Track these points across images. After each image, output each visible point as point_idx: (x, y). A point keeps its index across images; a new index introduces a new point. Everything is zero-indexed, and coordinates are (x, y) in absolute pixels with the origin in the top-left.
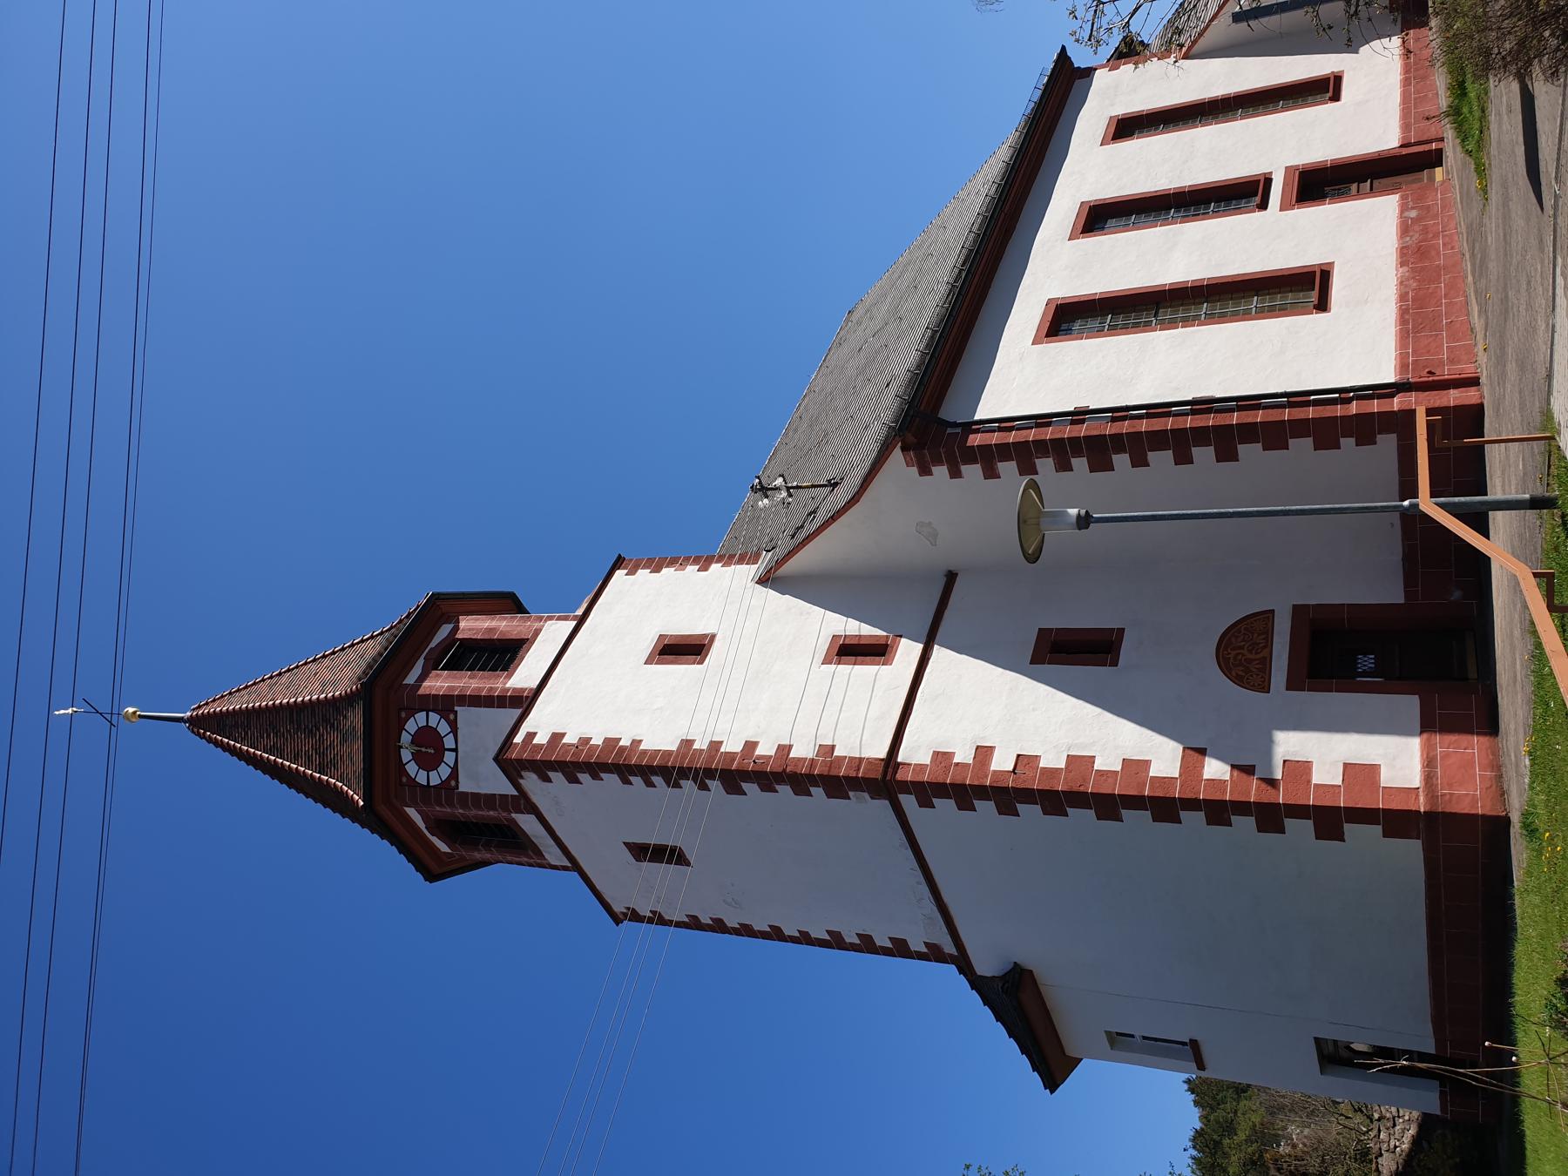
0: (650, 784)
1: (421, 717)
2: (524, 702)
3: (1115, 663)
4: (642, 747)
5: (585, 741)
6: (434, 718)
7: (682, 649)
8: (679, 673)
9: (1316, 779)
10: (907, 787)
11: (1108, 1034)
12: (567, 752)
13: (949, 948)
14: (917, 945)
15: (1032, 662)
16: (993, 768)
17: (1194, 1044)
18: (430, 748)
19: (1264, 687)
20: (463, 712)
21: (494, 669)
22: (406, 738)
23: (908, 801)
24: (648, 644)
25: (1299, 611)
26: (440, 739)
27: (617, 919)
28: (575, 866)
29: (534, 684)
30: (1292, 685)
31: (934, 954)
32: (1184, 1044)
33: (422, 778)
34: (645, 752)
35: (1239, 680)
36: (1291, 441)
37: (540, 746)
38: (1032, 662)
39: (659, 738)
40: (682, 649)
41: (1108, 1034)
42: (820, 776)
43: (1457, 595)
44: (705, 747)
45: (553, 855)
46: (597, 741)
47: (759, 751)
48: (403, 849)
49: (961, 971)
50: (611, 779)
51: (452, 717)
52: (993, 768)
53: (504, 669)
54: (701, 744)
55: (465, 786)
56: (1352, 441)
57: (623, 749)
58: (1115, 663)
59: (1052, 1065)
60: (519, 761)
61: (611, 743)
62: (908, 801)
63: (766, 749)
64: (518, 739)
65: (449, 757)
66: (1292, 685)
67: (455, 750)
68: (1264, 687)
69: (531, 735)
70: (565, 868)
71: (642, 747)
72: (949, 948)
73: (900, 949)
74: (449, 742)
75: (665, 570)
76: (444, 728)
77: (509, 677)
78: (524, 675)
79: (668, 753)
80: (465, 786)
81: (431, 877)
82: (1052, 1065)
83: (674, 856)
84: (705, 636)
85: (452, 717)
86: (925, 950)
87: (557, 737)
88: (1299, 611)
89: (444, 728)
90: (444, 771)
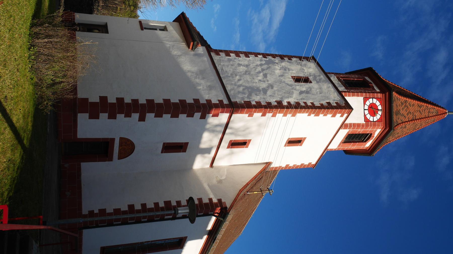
0: (305, 103)
1: (376, 119)
2: (344, 125)
3: (164, 144)
4: (307, 114)
5: (325, 115)
6: (371, 119)
7: (295, 142)
8: (296, 135)
9: (107, 115)
10: (227, 106)
11: (167, 30)
12: (330, 112)
13: (213, 54)
14: (223, 54)
15: (188, 143)
16: (200, 113)
17: (142, 28)
18: (373, 110)
19: (121, 139)
20: (362, 121)
21: (353, 134)
22: (380, 113)
23: (226, 102)
24: (305, 143)
25: (111, 159)
26: (369, 113)
27: (314, 58)
28: (326, 74)
29: (341, 130)
30: (113, 140)
31: (217, 52)
32: (145, 28)
33: (375, 101)
34: (307, 113)
35: (128, 140)
36: (113, 211)
37: (339, 113)
38: (188, 143)
39: (302, 117)
40: (295, 142)
41: (167, 30)
42: (252, 108)
43: (66, 165)
44: (288, 115)
45: (334, 79)
46: (321, 115)
47: (271, 114)
48: (378, 77)
49: (209, 46)
50: (317, 104)
51: (366, 120)
52: (200, 113)
53: (349, 135)
54: (289, 116)
55: (361, 99)
56: (95, 212)
57: (313, 113)
58: (164, 144)
59: (182, 20)
60: (345, 109)
61: (317, 115)
62: (226, 102)
63: (269, 115)
64: (346, 115)
65: (366, 107)
66: (113, 140)
67: (365, 110)
68: (121, 139)
69: (342, 116)
70: (329, 73)
71: (307, 114)
72: (213, 54)
73: (228, 53)
74: (367, 112)
75: (300, 164)
76: (368, 116)
77: (348, 132)
78: (344, 133)
79: (300, 112)
80: (361, 99)
81: (370, 69)
82: (182, 20)
83: (298, 80)
84: (288, 146)
85: (366, 120)
86: (220, 53)
87: (334, 116)
88: (111, 159)
89: (368, 116)
90: (368, 103)
